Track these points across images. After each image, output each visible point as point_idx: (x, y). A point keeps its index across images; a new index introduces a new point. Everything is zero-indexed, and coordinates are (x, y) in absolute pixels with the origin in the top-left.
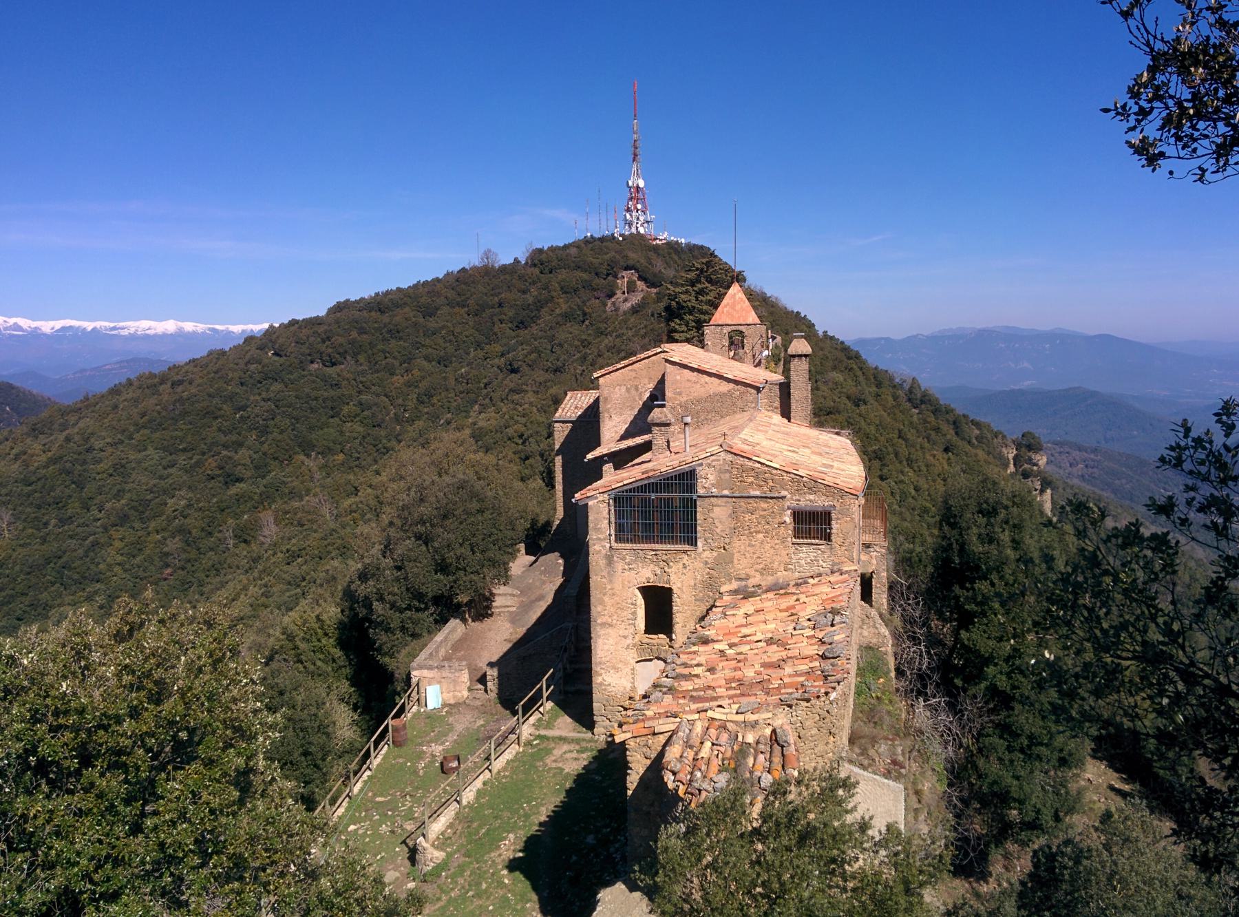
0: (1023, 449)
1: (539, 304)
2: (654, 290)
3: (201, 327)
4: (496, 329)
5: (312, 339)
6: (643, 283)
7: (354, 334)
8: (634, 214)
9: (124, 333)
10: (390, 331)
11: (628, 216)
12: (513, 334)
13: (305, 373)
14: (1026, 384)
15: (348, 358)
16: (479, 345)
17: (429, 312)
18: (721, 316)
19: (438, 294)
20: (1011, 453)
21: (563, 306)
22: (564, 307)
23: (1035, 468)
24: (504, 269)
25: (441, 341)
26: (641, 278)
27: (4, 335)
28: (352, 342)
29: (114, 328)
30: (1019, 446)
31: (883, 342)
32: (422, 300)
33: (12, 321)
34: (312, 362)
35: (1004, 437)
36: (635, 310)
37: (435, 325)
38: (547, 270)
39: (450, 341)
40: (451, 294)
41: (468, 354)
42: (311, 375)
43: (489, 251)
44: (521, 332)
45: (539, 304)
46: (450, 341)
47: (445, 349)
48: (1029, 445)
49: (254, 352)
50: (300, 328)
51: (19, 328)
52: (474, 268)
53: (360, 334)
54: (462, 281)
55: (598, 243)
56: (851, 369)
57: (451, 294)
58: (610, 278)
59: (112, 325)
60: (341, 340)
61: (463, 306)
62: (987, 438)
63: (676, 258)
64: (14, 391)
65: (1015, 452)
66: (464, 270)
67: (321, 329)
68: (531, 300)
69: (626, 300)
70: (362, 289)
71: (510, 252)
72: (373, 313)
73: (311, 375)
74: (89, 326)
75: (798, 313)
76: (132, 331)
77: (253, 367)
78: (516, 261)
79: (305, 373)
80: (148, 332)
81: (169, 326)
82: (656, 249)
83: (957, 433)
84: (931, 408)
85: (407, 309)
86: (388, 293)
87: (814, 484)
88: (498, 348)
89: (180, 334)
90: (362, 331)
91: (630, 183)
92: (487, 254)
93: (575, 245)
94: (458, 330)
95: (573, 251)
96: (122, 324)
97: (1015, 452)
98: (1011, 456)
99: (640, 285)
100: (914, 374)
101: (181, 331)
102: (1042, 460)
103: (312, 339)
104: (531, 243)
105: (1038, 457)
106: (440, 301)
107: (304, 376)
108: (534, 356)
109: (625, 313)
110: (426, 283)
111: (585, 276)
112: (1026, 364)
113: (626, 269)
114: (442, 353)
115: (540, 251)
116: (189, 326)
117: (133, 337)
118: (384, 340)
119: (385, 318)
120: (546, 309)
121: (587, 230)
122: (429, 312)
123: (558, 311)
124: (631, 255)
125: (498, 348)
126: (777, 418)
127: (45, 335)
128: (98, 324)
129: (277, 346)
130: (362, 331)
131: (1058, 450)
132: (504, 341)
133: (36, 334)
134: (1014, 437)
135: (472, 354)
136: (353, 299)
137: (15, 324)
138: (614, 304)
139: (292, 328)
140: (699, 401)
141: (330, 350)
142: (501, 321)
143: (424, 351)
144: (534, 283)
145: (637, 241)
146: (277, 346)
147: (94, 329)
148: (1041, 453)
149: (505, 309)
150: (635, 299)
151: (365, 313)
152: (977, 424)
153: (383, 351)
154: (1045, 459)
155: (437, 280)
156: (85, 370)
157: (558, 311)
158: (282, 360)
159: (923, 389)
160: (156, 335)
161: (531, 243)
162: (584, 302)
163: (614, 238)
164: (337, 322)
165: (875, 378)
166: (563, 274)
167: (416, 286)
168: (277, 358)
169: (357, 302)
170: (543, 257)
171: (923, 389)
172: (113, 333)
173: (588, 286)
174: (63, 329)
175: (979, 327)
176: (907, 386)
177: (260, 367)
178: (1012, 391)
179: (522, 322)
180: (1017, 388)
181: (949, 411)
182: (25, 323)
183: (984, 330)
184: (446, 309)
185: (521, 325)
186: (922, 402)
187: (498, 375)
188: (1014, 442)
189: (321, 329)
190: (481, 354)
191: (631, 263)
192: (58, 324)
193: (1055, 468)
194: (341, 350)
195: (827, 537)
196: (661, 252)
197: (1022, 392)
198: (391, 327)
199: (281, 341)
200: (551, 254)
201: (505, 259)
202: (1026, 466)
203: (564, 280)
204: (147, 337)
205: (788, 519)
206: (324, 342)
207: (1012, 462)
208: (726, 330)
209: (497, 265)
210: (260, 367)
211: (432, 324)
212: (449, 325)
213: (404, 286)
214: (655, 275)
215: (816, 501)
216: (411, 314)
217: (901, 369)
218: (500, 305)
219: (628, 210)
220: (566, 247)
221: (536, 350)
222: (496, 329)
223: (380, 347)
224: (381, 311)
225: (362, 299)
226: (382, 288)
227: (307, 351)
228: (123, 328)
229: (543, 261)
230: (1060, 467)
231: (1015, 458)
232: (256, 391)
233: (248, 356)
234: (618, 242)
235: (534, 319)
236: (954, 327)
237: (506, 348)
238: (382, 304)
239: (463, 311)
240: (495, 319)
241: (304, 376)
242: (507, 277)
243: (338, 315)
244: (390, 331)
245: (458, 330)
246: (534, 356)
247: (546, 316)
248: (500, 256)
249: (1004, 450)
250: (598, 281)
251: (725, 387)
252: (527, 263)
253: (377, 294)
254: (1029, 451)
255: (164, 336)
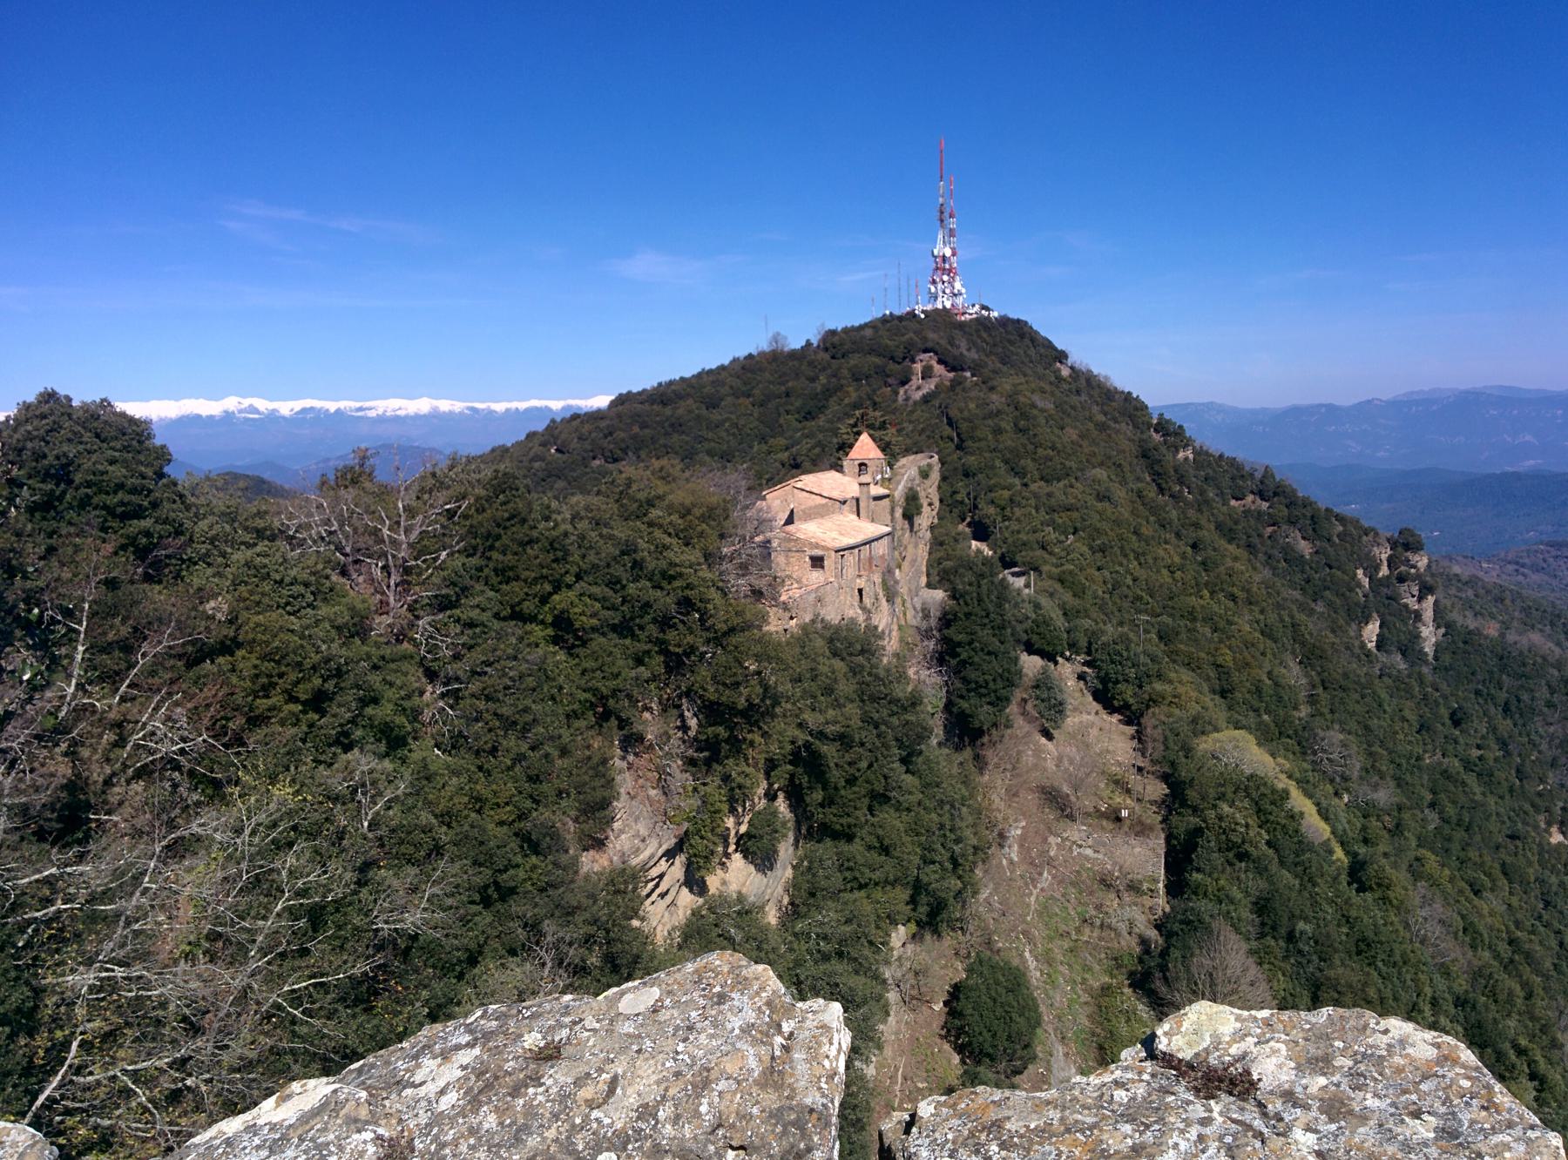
0: (1400, 549)
1: (828, 393)
2: (951, 375)
3: (458, 406)
4: (781, 421)
5: (594, 435)
6: (942, 367)
7: (636, 429)
8: (940, 286)
9: (372, 414)
10: (672, 425)
11: (933, 290)
12: (800, 426)
13: (588, 470)
14: (1529, 464)
15: (630, 454)
16: (763, 439)
17: (712, 404)
18: (854, 454)
19: (723, 384)
20: (1384, 554)
21: (853, 394)
22: (854, 395)
23: (1413, 571)
24: (793, 355)
25: (724, 434)
26: (940, 362)
27: (238, 419)
28: (634, 437)
29: (360, 409)
30: (1394, 544)
31: (1323, 410)
32: (706, 390)
33: (247, 402)
34: (594, 458)
35: (1377, 534)
36: (926, 399)
37: (719, 417)
38: (839, 355)
39: (734, 434)
40: (737, 383)
41: (751, 447)
42: (593, 472)
43: (778, 334)
44: (808, 424)
45: (828, 393)
46: (734, 434)
47: (728, 442)
48: (1406, 543)
49: (537, 449)
50: (582, 422)
51: (256, 411)
52: (762, 354)
53: (642, 428)
54: (748, 368)
55: (896, 322)
56: (1120, 466)
57: (737, 383)
58: (907, 361)
59: (358, 405)
60: (622, 435)
61: (749, 396)
62: (1355, 534)
63: (985, 335)
64: (265, 486)
65: (1389, 552)
66: (750, 356)
67: (603, 424)
68: (819, 388)
69: (919, 388)
70: (643, 379)
71: (799, 334)
72: (655, 407)
73: (593, 472)
74: (332, 406)
75: (1129, 393)
76: (380, 412)
77: (537, 465)
78: (808, 343)
79: (588, 470)
80: (399, 413)
81: (422, 406)
82: (962, 326)
83: (1314, 529)
84: (1284, 501)
85: (690, 401)
86: (671, 383)
87: (817, 546)
88: (782, 441)
89: (435, 415)
90: (644, 426)
91: (936, 252)
92: (776, 338)
93: (870, 325)
94: (742, 422)
95: (868, 332)
96: (367, 404)
97: (1389, 552)
98: (1384, 557)
99: (939, 369)
100: (1267, 462)
101: (435, 409)
102: (1422, 561)
103: (594, 435)
104: (823, 325)
105: (1417, 558)
106: (724, 390)
107: (587, 473)
108: (817, 450)
109: (915, 403)
110: (710, 372)
111: (877, 360)
112: (1528, 438)
113: (926, 351)
114: (725, 447)
115: (833, 333)
116: (445, 405)
117: (382, 420)
118: (667, 434)
119: (668, 411)
120: (835, 398)
121: (886, 308)
122: (712, 404)
123: (847, 401)
124: (931, 335)
125: (782, 441)
126: (854, 517)
127: (284, 418)
128: (343, 404)
129: (559, 442)
130: (644, 426)
131: (1554, 553)
132: (790, 433)
133: (273, 418)
134: (1389, 535)
135: (755, 449)
136: (635, 391)
137: (251, 406)
138: (906, 392)
139: (575, 423)
140: (810, 508)
141: (612, 446)
142: (788, 412)
143: (707, 445)
144: (824, 369)
145: (942, 318)
146: (559, 442)
147: (338, 411)
148: (1422, 553)
149: (792, 399)
150: (930, 386)
151: (647, 407)
152: (1341, 519)
153: (665, 446)
154: (1425, 561)
155: (722, 368)
156: (328, 460)
157: (847, 401)
158: (565, 457)
159: (1278, 479)
160: (407, 417)
161: (823, 325)
162: (874, 391)
163: (915, 316)
164: (619, 416)
165: (1176, 471)
166: (854, 360)
167: (699, 375)
168: (559, 455)
169: (639, 393)
170: (836, 339)
171: (1278, 479)
172: (360, 414)
173: (882, 373)
174: (304, 410)
175: (1463, 387)
176: (1258, 475)
177: (543, 465)
178: (1505, 474)
179: (809, 413)
180: (1510, 469)
181: (1306, 503)
182: (263, 405)
183: (1467, 392)
184: (729, 399)
185: (809, 416)
186: (1276, 494)
187: (779, 470)
188: (1388, 540)
189: (603, 424)
190: (764, 448)
191: (929, 345)
192: (298, 405)
193: (1546, 578)
194: (623, 446)
195: (823, 567)
196: (967, 329)
197: (1517, 476)
198: (673, 420)
199: (563, 436)
200: (843, 335)
201: (796, 343)
202: (1403, 568)
203: (856, 366)
204: (397, 420)
205: (807, 559)
206: (606, 437)
207: (1385, 563)
208: (857, 463)
209: (786, 349)
210: (543, 465)
211: (715, 416)
212: (733, 417)
213: (688, 375)
214: (955, 358)
215: (818, 552)
216: (694, 407)
217: (1251, 455)
218: (788, 395)
219: (934, 282)
220: (862, 327)
221: (819, 444)
222: (781, 421)
223: (662, 442)
224: (664, 403)
225: (644, 391)
226: (665, 378)
227: (589, 447)
228: (370, 409)
229: (836, 345)
230: (1555, 576)
231: (1390, 560)
232: (540, 489)
233: (532, 454)
234: (920, 321)
235: (822, 409)
236: (1426, 389)
237: (790, 442)
238: (665, 395)
239: (747, 402)
240: (781, 410)
241: (587, 473)
242: (795, 363)
243: (620, 408)
244: (672, 425)
245: (742, 422)
246: (817, 450)
247: (834, 407)
248: (790, 339)
249: (1376, 550)
250: (892, 366)
251: (824, 501)
252: (818, 346)
253: (660, 384)
254: (1406, 550)
255: (417, 418)
